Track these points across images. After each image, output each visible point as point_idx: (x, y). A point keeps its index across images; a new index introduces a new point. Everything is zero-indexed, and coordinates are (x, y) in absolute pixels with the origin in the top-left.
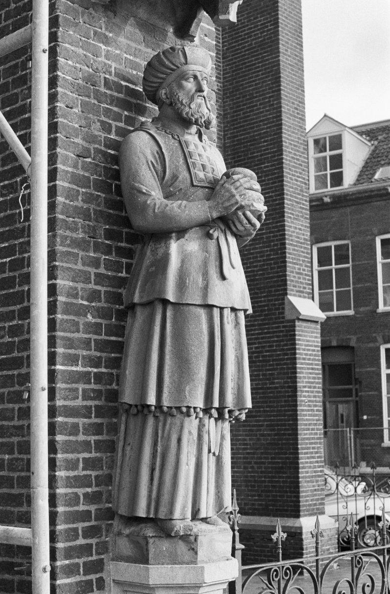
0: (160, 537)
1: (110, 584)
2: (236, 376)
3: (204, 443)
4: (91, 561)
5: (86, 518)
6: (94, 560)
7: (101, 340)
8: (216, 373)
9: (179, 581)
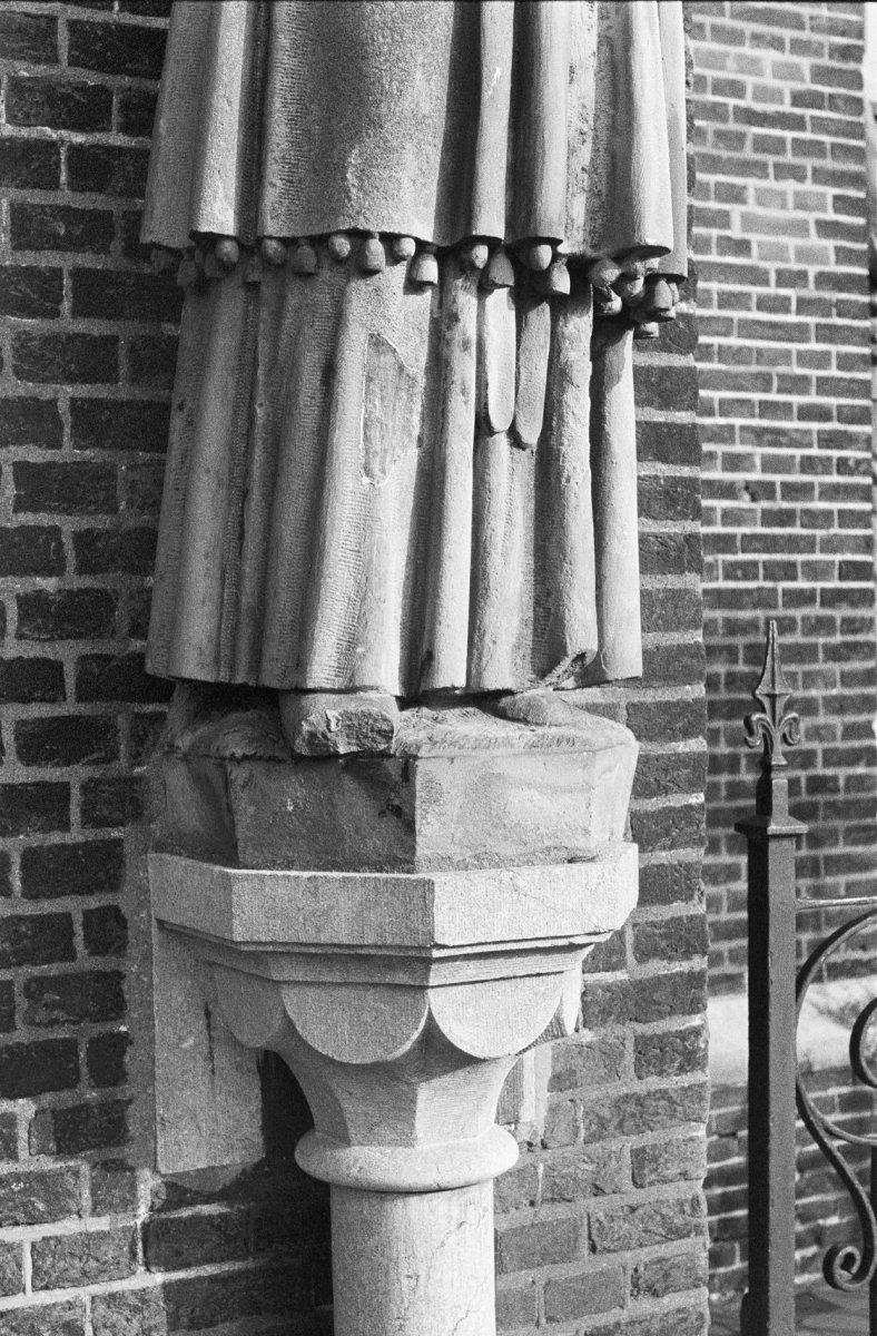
0: (273, 759)
1: (148, 934)
2: (604, 121)
3: (456, 388)
4: (63, 847)
5: (35, 690)
6: (75, 847)
7: (105, 26)
8: (487, 95)
9: (340, 931)
